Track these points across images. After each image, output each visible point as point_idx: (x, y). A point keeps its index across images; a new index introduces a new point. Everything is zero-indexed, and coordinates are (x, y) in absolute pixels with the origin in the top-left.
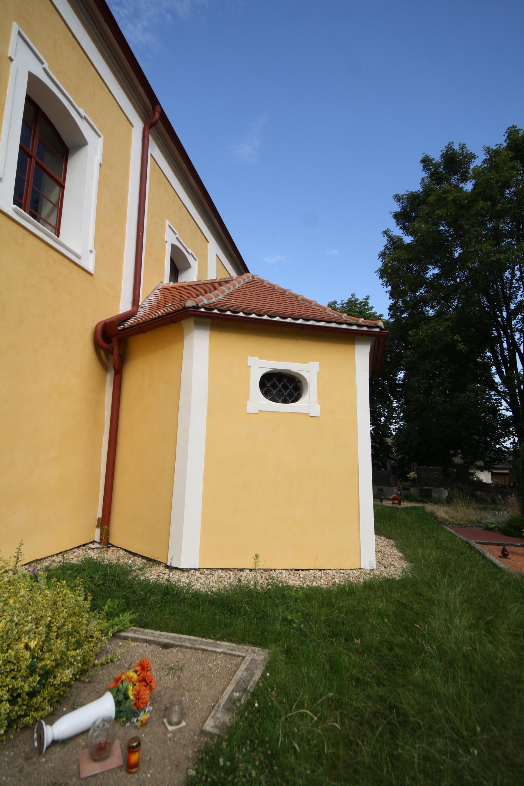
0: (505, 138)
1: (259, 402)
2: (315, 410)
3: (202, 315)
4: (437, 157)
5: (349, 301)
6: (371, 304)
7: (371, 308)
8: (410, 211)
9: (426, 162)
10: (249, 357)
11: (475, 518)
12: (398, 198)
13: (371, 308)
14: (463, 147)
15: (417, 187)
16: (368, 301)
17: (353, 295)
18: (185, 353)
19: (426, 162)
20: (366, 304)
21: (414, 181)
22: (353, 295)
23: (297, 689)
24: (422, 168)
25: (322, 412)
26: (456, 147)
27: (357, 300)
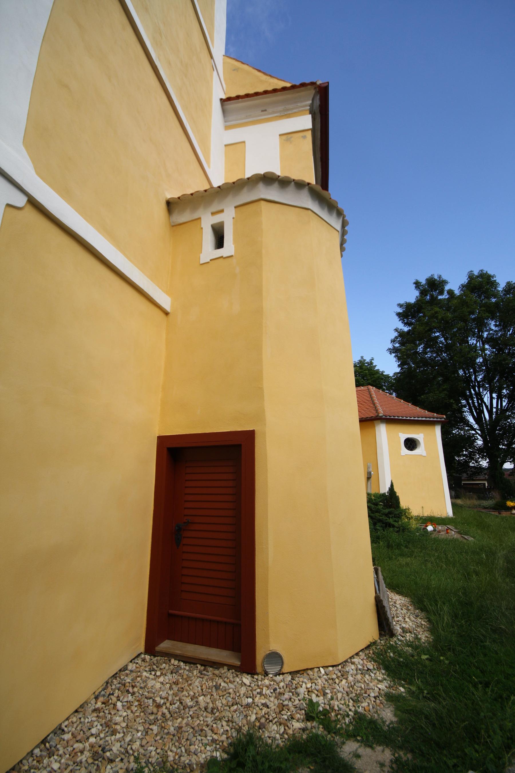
0: (467, 277)
1: (405, 451)
2: (424, 454)
3: (384, 419)
4: (423, 281)
5: (360, 361)
6: (375, 363)
7: (375, 366)
8: (408, 313)
9: (417, 284)
10: (400, 434)
11: (264, 702)
12: (400, 306)
13: (375, 366)
14: (440, 277)
15: (412, 300)
16: (373, 361)
17: (362, 357)
18: (377, 433)
19: (417, 284)
20: (371, 363)
21: (412, 296)
22: (362, 357)
23: (333, 689)
24: (414, 288)
25: (427, 454)
26: (436, 277)
27: (365, 360)
